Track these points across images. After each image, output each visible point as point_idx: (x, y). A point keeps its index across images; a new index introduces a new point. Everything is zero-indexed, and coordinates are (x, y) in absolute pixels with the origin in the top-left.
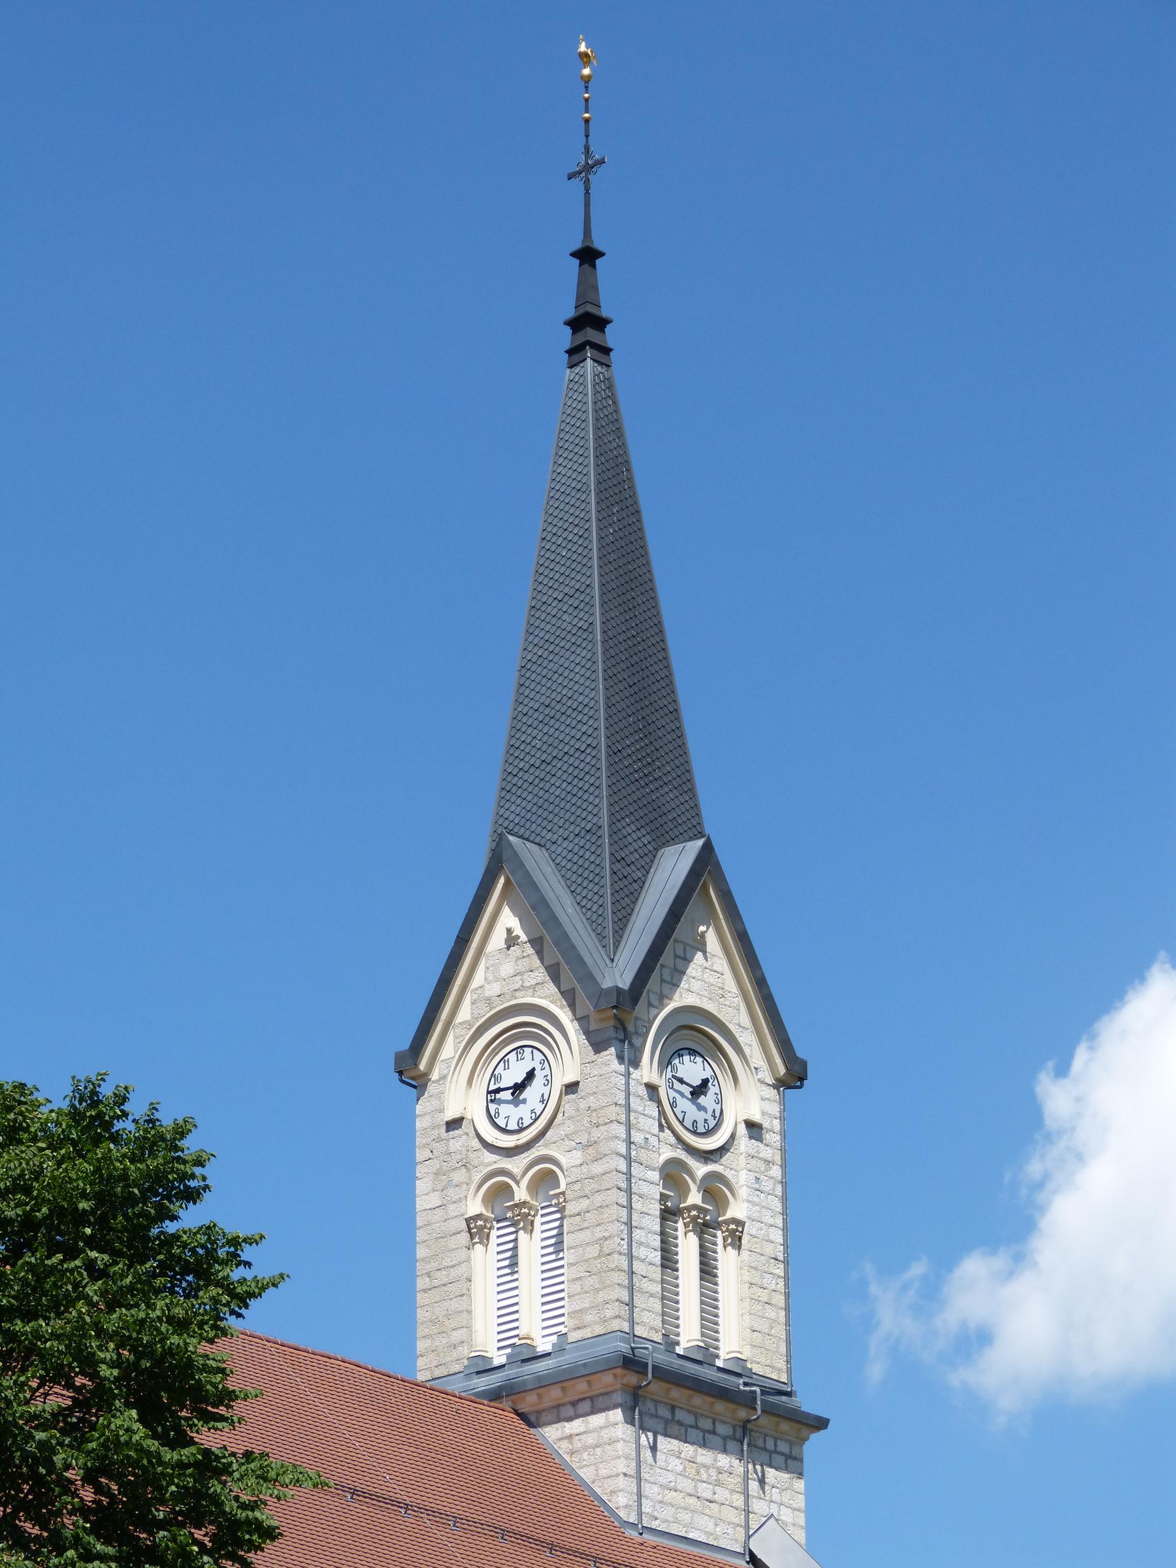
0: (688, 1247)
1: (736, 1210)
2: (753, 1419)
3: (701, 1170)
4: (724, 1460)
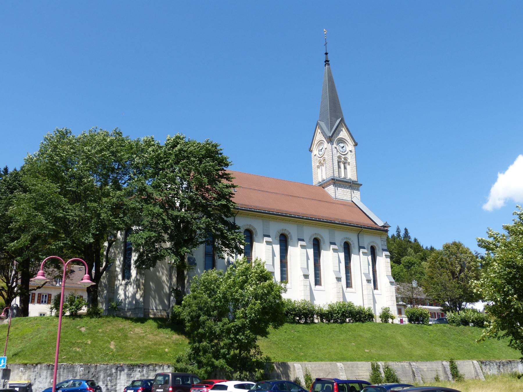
0: (342, 166)
1: (349, 161)
2: (353, 185)
3: (343, 156)
4: (348, 190)
